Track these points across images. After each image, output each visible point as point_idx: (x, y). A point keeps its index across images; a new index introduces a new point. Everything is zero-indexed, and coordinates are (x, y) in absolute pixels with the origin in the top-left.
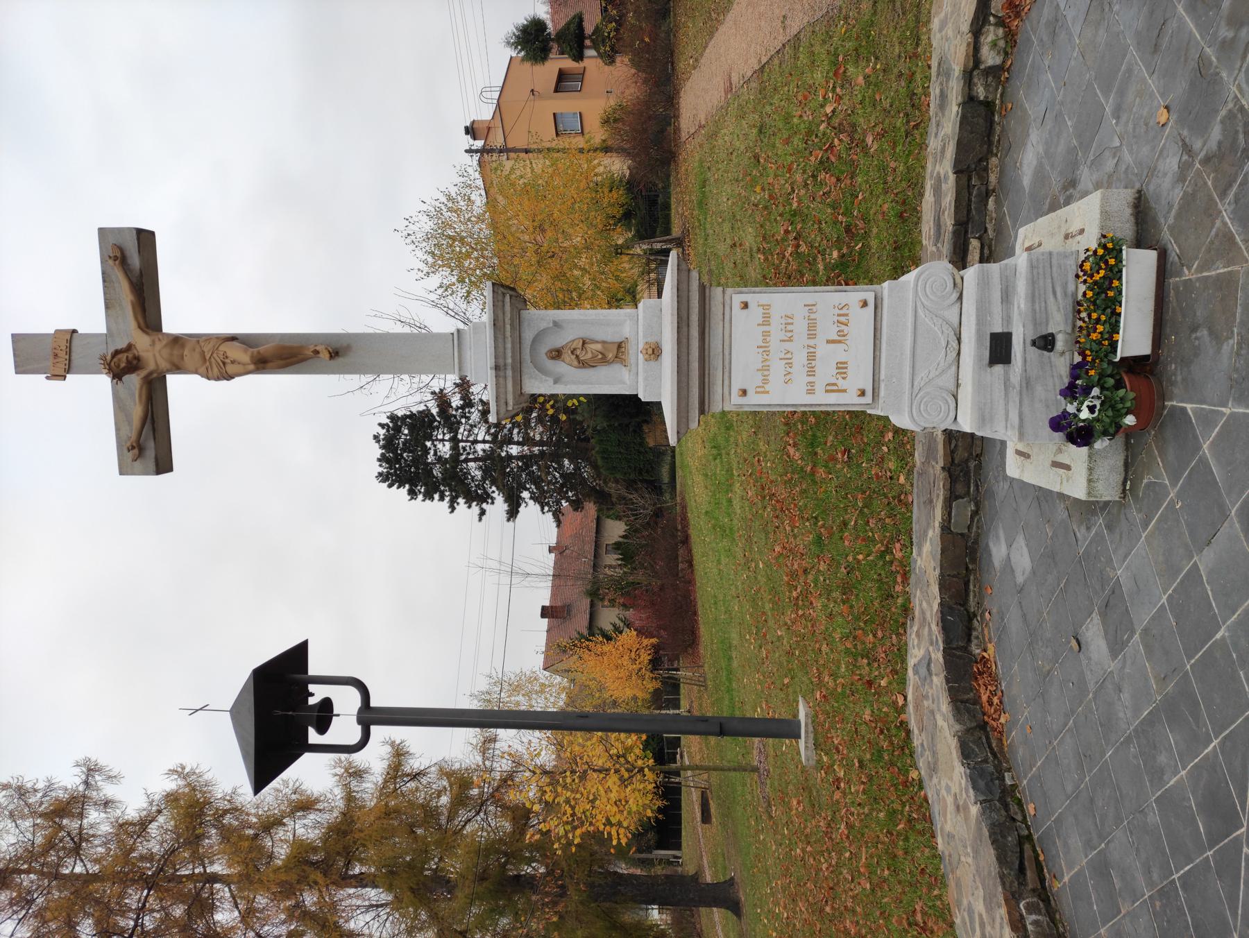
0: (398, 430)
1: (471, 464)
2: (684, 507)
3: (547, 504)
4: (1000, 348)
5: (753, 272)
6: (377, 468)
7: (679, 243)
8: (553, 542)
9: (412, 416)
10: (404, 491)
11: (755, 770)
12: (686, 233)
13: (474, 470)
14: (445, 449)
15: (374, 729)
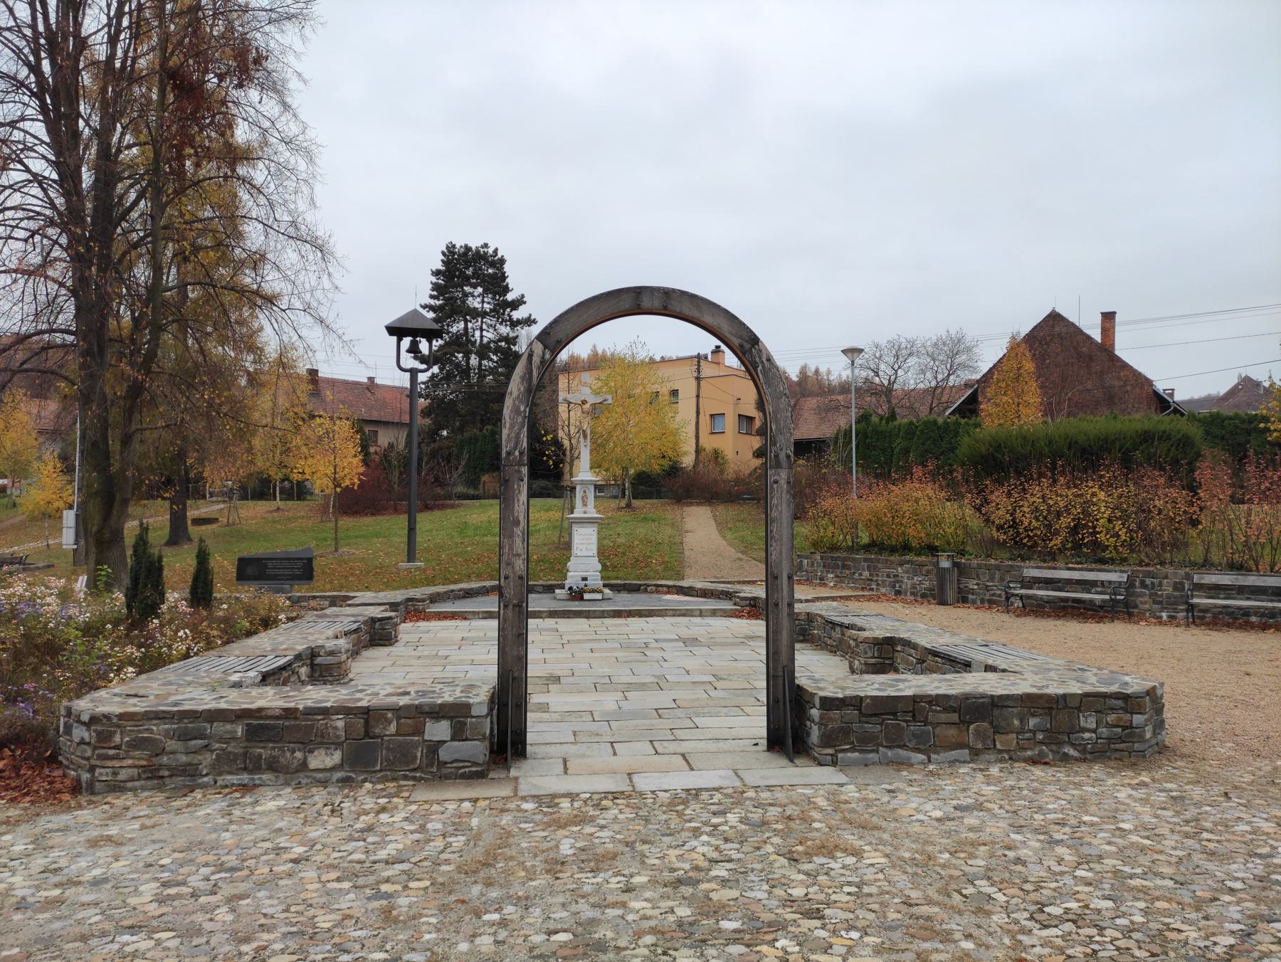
0: (492, 264)
1: (462, 325)
2: (452, 506)
3: (427, 387)
4: (584, 579)
5: (606, 542)
6: (459, 243)
7: (628, 506)
8: (378, 381)
9: (504, 277)
10: (440, 266)
11: (336, 550)
12: (634, 509)
13: (458, 327)
14: (475, 303)
15: (408, 374)
